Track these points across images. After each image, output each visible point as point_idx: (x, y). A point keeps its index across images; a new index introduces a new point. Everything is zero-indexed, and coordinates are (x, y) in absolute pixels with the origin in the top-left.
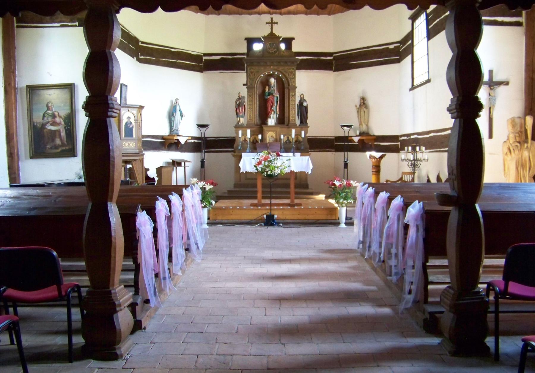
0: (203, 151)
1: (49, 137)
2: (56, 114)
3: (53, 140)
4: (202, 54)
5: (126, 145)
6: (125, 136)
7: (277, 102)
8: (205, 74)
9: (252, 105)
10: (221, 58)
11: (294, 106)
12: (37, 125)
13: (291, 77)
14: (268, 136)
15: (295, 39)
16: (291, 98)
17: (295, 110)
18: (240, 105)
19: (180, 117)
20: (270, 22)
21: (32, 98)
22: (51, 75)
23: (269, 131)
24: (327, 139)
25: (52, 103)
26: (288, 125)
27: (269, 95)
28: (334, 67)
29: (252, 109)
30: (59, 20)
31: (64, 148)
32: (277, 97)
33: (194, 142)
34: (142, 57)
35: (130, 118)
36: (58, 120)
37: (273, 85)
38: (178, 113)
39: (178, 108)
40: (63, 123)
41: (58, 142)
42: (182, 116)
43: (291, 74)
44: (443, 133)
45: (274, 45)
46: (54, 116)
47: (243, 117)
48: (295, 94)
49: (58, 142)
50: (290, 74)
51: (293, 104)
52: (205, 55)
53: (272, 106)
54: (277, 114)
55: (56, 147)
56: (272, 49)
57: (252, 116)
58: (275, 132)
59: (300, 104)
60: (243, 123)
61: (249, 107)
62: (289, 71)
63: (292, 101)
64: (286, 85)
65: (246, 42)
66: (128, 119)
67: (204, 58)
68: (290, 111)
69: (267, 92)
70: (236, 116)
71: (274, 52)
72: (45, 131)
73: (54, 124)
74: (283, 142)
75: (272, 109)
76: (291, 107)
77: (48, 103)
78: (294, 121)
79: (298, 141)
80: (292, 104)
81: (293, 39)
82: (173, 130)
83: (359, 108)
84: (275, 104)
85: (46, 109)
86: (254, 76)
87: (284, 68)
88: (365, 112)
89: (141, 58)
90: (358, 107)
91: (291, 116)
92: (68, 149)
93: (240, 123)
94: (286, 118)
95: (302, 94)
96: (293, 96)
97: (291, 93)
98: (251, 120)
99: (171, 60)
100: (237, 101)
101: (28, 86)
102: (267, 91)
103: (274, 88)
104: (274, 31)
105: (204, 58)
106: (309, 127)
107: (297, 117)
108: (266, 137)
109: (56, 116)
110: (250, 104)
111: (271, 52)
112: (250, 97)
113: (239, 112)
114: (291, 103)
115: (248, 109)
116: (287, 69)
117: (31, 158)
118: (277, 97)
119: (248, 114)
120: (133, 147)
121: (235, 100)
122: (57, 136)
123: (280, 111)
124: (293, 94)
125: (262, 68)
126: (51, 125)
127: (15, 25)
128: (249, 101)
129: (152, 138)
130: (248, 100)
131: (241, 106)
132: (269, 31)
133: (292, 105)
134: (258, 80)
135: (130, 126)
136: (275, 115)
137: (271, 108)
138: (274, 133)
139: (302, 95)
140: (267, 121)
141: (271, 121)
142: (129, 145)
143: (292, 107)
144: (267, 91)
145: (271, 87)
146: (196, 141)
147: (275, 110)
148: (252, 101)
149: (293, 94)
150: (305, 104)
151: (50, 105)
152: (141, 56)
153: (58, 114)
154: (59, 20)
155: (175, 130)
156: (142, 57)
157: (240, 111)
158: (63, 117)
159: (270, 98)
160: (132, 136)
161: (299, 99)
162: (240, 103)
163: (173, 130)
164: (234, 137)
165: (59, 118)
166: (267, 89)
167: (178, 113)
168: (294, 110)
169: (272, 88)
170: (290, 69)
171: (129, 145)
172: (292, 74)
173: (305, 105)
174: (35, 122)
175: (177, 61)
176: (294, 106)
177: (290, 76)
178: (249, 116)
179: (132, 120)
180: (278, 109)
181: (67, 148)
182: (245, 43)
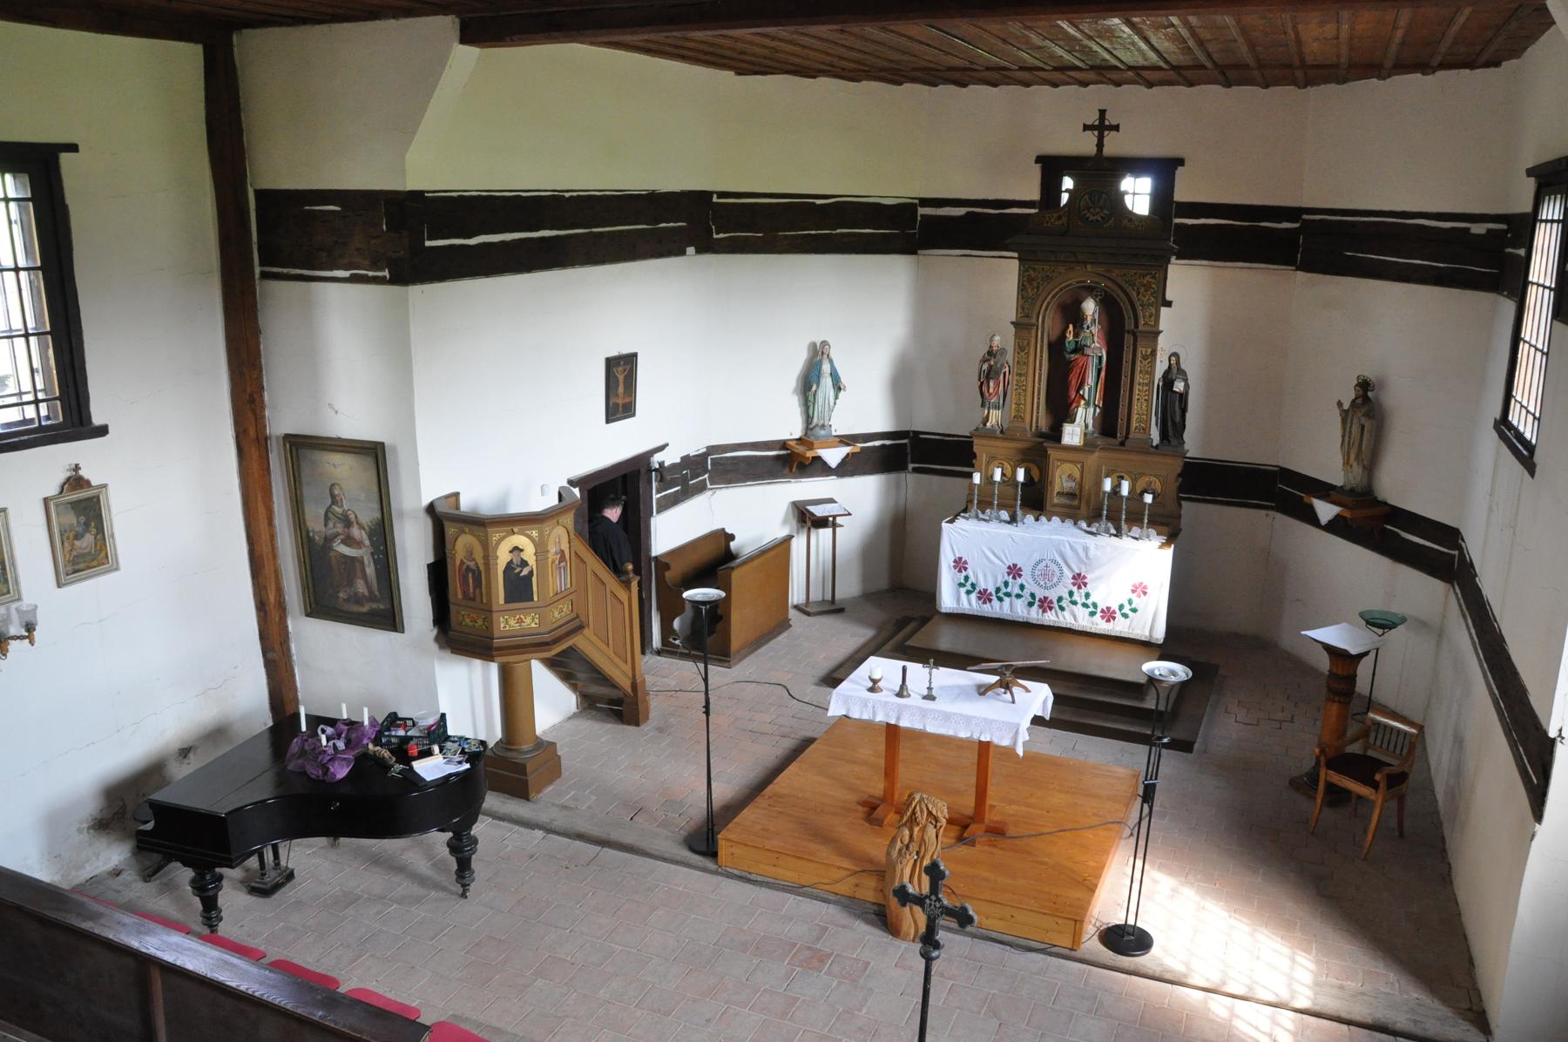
0: (911, 466)
1: (342, 570)
2: (352, 517)
3: (351, 583)
4: (917, 201)
5: (512, 622)
6: (507, 601)
7: (1099, 371)
8: (921, 257)
10: (968, 213)
11: (1145, 388)
12: (314, 537)
13: (1145, 299)
15: (1187, 162)
16: (1138, 364)
18: (992, 373)
19: (832, 393)
20: (1096, 133)
21: (299, 467)
22: (336, 412)
23: (1063, 461)
24: (1255, 469)
25: (341, 489)
26: (1122, 444)
27: (1075, 351)
28: (1299, 256)
29: (1024, 388)
30: (346, 261)
31: (375, 606)
33: (883, 446)
34: (721, 235)
35: (522, 550)
36: (356, 532)
38: (827, 382)
39: (826, 368)
40: (367, 542)
41: (361, 587)
42: (838, 387)
43: (1146, 290)
46: (348, 523)
47: (997, 407)
49: (361, 587)
50: (1142, 290)
51: (1145, 381)
52: (925, 202)
53: (1081, 386)
55: (358, 600)
59: (1164, 385)
61: (1017, 381)
62: (1140, 283)
63: (1141, 372)
64: (1129, 325)
65: (1038, 167)
66: (516, 553)
67: (922, 211)
68: (1135, 402)
69: (1069, 342)
71: (1103, 218)
72: (332, 554)
73: (349, 541)
75: (1081, 392)
76: (1136, 392)
77: (332, 485)
80: (1141, 381)
81: (1180, 162)
82: (811, 426)
83: (1348, 409)
85: (329, 502)
86: (1035, 290)
87: (1126, 271)
88: (1363, 427)
89: (718, 239)
90: (1346, 406)
91: (1135, 417)
92: (383, 609)
93: (988, 424)
95: (1175, 355)
96: (1145, 357)
97: (1141, 350)
99: (813, 232)
100: (984, 361)
101: (287, 437)
102: (1071, 338)
105: (922, 211)
108: (1053, 476)
109: (352, 523)
110: (1019, 372)
111: (1092, 218)
112: (1022, 351)
114: (1138, 378)
115: (1015, 387)
116: (1135, 274)
117: (308, 615)
120: (533, 625)
121: (980, 357)
122: (359, 575)
123: (1105, 398)
124: (1146, 352)
125: (1061, 269)
126: (344, 542)
127: (257, 270)
128: (1018, 362)
134: (1071, 284)
135: (521, 571)
136: (1091, 410)
137: (1078, 391)
138: (1076, 469)
139: (1174, 358)
142: (520, 621)
143: (1139, 390)
144: (1070, 337)
145: (1085, 326)
146: (888, 442)
147: (1089, 396)
149: (1146, 352)
150: (1179, 386)
151: (336, 492)
152: (717, 234)
153: (356, 517)
154: (346, 261)
155: (817, 425)
156: (721, 235)
157: (991, 390)
158: (366, 528)
160: (532, 600)
161: (1166, 366)
163: (811, 426)
165: (359, 528)
167: (827, 382)
170: (1144, 276)
171: (520, 621)
172: (1149, 293)
173: (1178, 390)
174: (310, 529)
175: (834, 232)
176: (1145, 388)
177: (1140, 296)
178: (1014, 406)
179: (529, 554)
180: (1100, 392)
181: (382, 607)
182: (1037, 170)
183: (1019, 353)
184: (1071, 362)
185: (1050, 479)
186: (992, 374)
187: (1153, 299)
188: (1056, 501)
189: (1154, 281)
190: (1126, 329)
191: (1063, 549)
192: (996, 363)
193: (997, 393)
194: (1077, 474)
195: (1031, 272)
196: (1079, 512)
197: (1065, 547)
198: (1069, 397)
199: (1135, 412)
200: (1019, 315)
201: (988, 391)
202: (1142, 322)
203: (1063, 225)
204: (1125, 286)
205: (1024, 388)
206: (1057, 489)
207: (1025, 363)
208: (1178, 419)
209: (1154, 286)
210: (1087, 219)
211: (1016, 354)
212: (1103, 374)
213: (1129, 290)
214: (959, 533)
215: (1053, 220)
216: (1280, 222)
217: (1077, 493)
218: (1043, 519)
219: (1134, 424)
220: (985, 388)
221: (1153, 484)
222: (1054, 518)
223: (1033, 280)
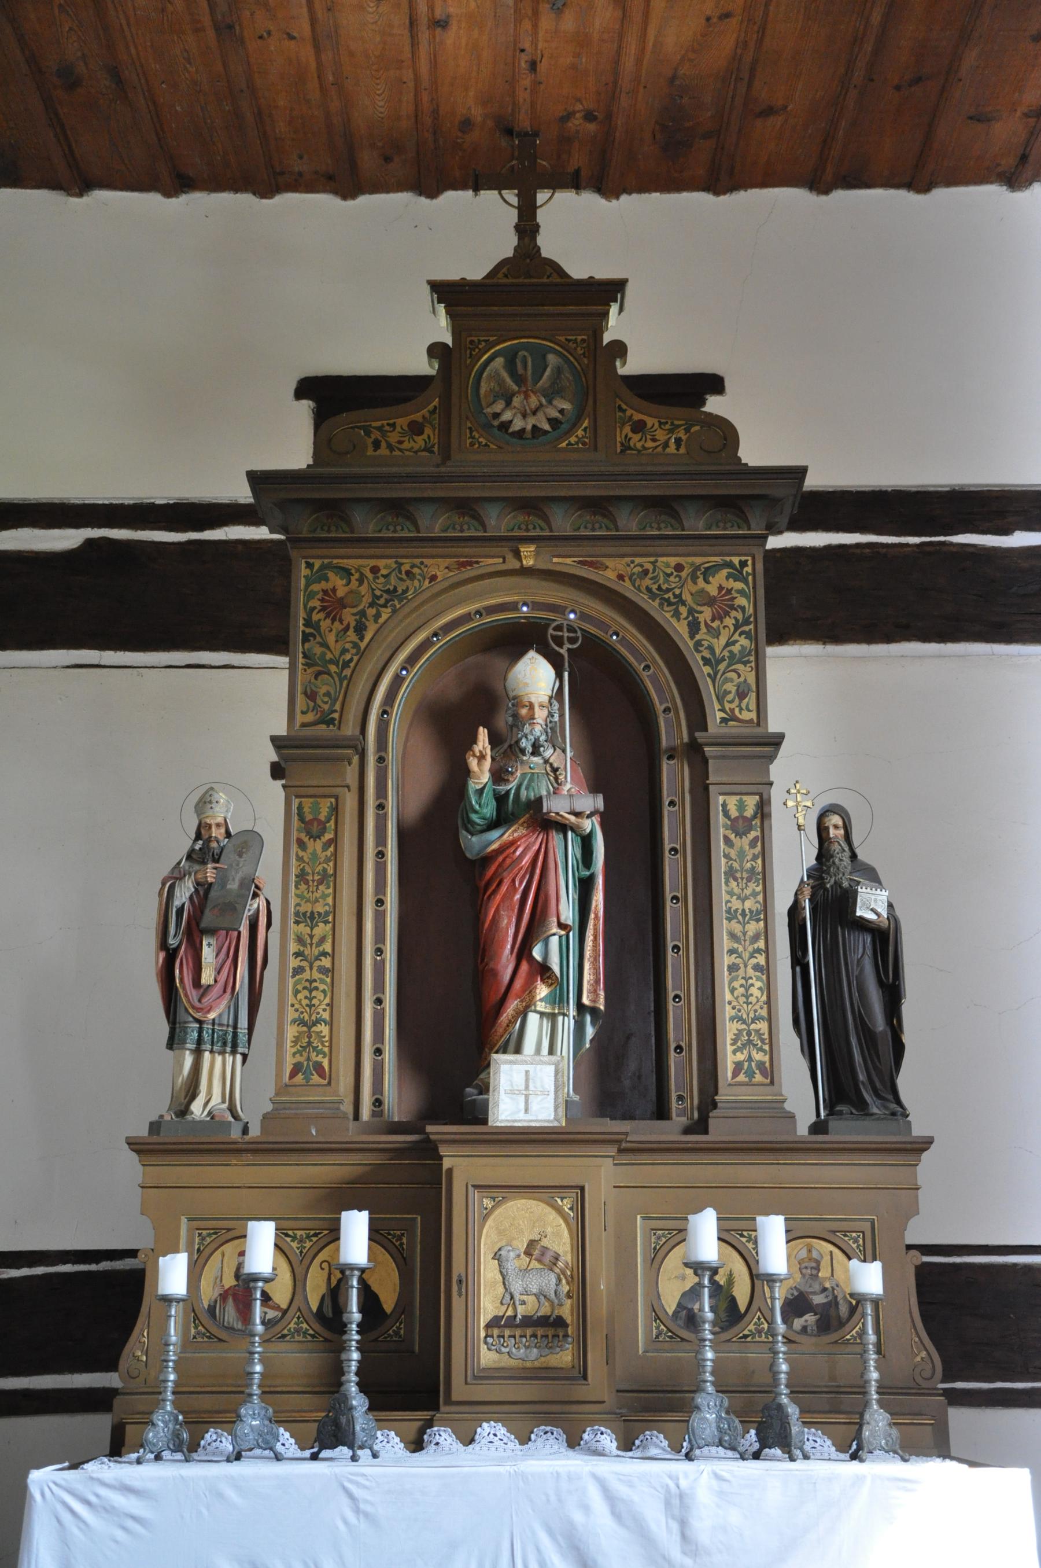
7: (585, 887)
9: (331, 916)
10: (89, 542)
11: (753, 927)
14: (488, 1240)
16: (718, 847)
17: (766, 970)
27: (500, 821)
29: (326, 962)
32: (586, 843)
37: (538, 730)
44: (105, 1265)
45: (551, 358)
47: (230, 1043)
48: (763, 810)
54: (580, 1007)
56: (534, 401)
57: (324, 1029)
58: (566, 1205)
60: (232, 1109)
61: (300, 940)
63: (731, 873)
65: (306, 406)
69: (480, 792)
70: (165, 1028)
71: (554, 422)
74: (656, 1312)
75: (537, 953)
76: (723, 942)
78: (758, 1078)
79: (818, 1299)
80: (736, 904)
84: (568, 912)
86: (351, 635)
87: (646, 562)
91: (728, 1030)
93: (197, 1108)
94: (679, 1048)
96: (739, 826)
98: (319, 1068)
102: (486, 778)
103: (548, 753)
104: (549, 245)
106: (925, 1144)
107: (789, 1041)
110: (306, 908)
111: (518, 424)
113: (194, 994)
115: (294, 963)
116: (679, 568)
118: (586, 843)
119: (291, 1015)
124: (741, 806)
128: (302, 876)
129: (74, 1263)
130: (294, 871)
131: (212, 932)
132: (506, 245)
133: (731, 915)
136: (566, 1025)
137: (523, 952)
138: (552, 1216)
139: (836, 819)
140: (484, 1089)
141: (519, 1080)
143: (733, 936)
144: (481, 773)
148: (326, 878)
157: (207, 977)
159: (513, 843)
162: (203, 890)
164: (133, 1253)
166: (482, 757)
168: (757, 968)
169: (536, 751)
170: (708, 572)
172: (729, 622)
173: (871, 916)
176: (753, 927)
178: (291, 1031)
183: (301, 844)
184: (487, 860)
185: (458, 1268)
186: (208, 919)
187: (744, 642)
188: (487, 1357)
189: (739, 585)
190: (664, 743)
191: (578, 1517)
192: (223, 877)
193: (230, 986)
194: (560, 1241)
195: (336, 581)
196: (581, 1392)
197: (586, 1508)
198: (495, 974)
199: (729, 1012)
200: (299, 719)
201: (197, 982)
202: (715, 715)
203: (428, 449)
204: (652, 607)
205: (326, 962)
206: (489, 1306)
207: (324, 874)
208: (879, 1023)
209: (742, 601)
210: (505, 426)
211: (294, 848)
212: (598, 898)
213: (664, 617)
214: (107, 1510)
215: (393, 438)
216: (1006, 531)
217: (566, 1311)
218: (444, 1436)
219: (729, 1057)
220: (182, 974)
221: (824, 1273)
222: (486, 1429)
223: (342, 604)
